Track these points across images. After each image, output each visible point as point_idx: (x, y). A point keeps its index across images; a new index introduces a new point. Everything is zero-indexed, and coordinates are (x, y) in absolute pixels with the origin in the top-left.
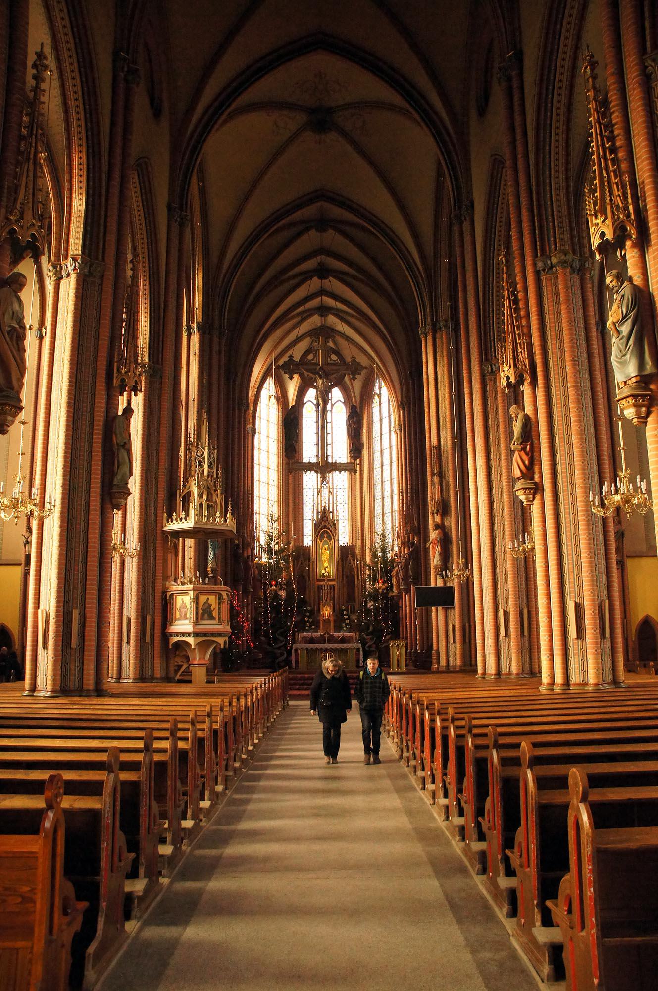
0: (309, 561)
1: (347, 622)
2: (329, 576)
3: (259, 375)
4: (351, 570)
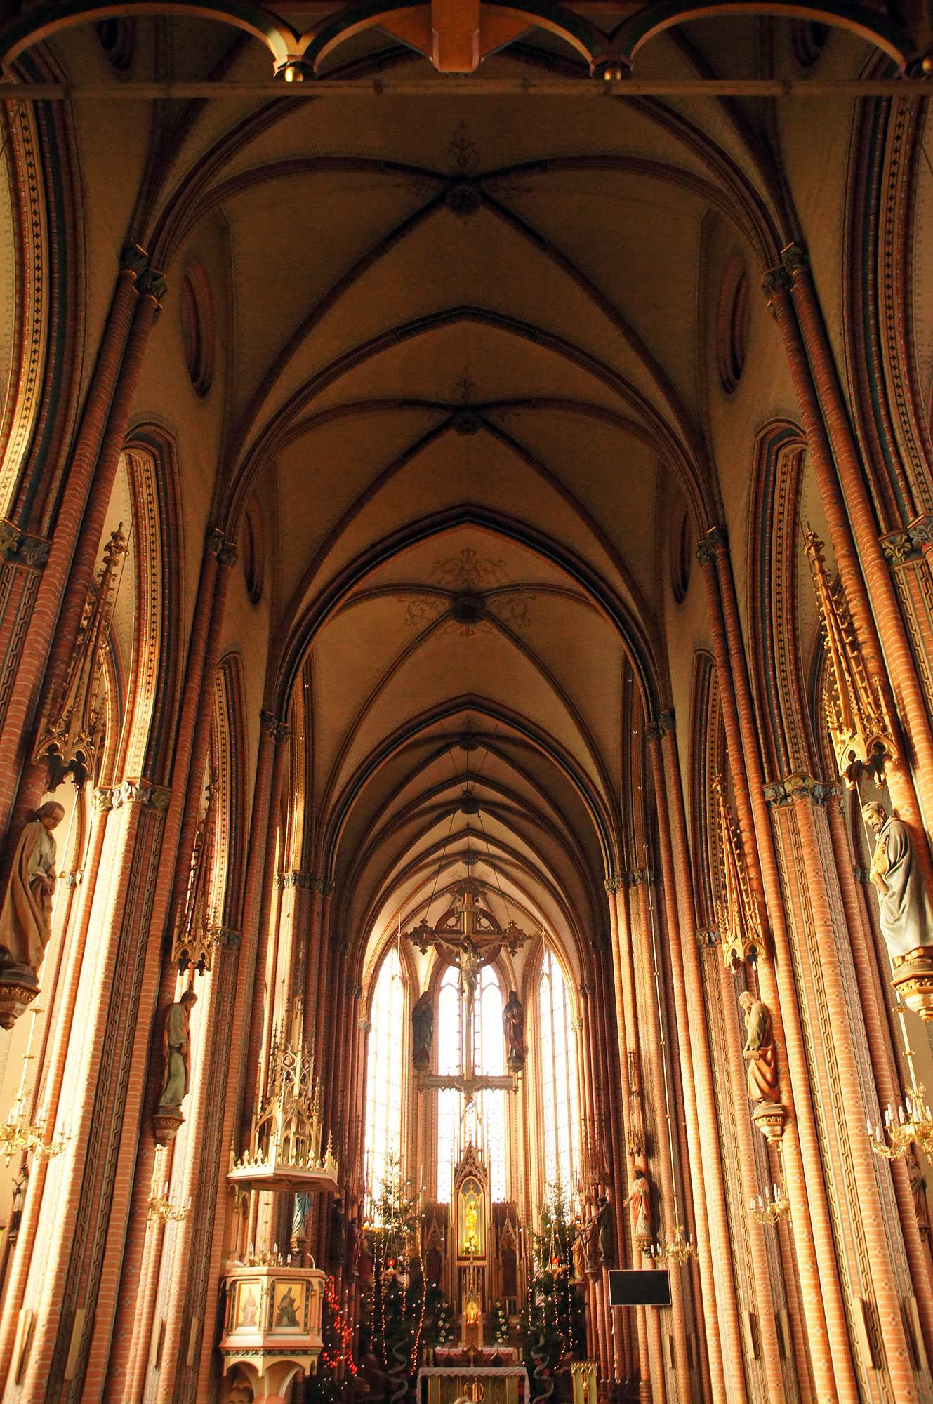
0: (446, 1228)
1: (504, 1328)
4: (510, 1242)
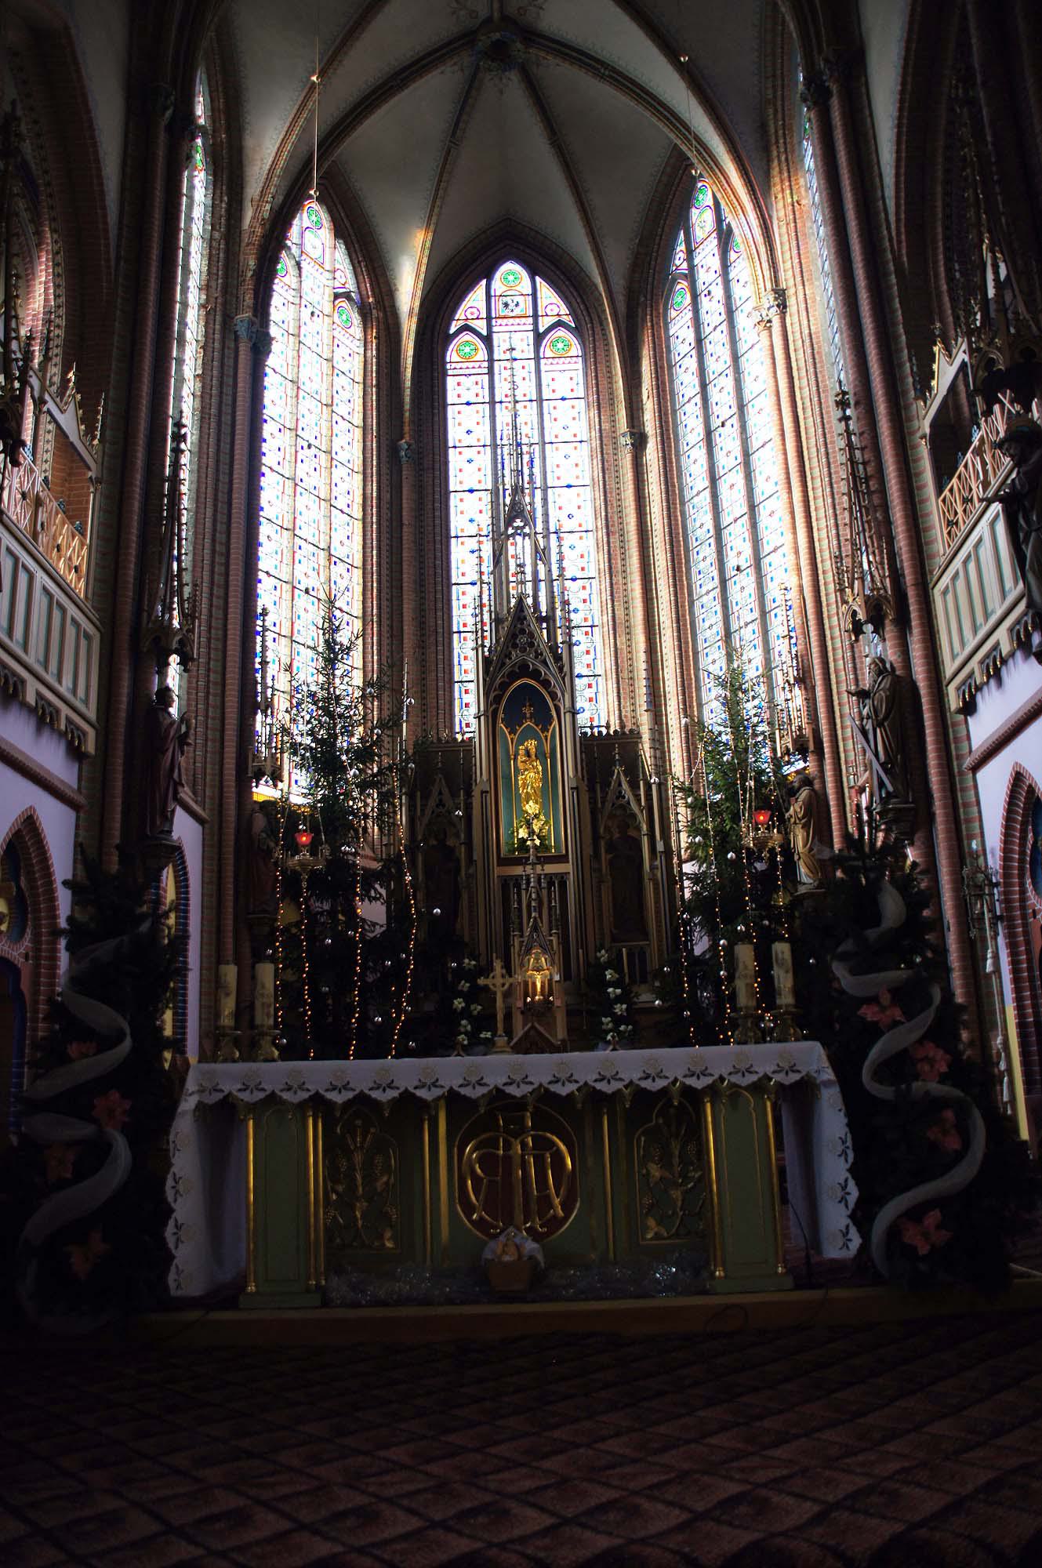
0: (469, 794)
1: (620, 1009)
2: (544, 846)
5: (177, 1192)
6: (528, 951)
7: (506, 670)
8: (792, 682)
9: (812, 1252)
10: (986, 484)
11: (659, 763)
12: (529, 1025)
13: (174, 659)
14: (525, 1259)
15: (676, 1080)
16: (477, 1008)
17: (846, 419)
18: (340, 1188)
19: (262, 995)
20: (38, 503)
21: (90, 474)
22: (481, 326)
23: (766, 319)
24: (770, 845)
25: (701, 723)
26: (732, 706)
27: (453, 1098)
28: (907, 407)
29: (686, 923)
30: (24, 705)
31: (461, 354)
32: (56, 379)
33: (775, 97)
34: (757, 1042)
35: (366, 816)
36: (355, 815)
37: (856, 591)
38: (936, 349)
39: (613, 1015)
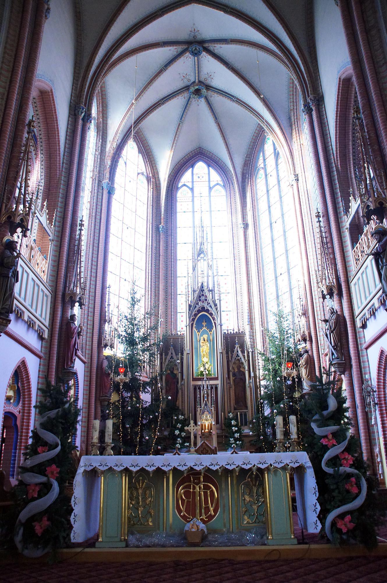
0: (182, 354)
1: (237, 435)
2: (209, 374)
3: (120, 125)
4: (240, 364)
5: (75, 503)
6: (203, 413)
7: (197, 309)
8: (301, 315)
9: (304, 531)
10: (369, 247)
11: (252, 344)
12: (203, 442)
13: (77, 304)
14: (200, 530)
15: (255, 465)
16: (183, 434)
17: (319, 222)
18: (133, 502)
19: (108, 431)
20: (32, 249)
21: (50, 238)
22: (190, 185)
23: (291, 184)
24: (292, 375)
25: (267, 330)
26: (279, 323)
27: (175, 470)
28: (341, 218)
29: (262, 404)
30: (23, 320)
31: (183, 195)
32: (40, 205)
33: (294, 109)
34: (284, 452)
35: (144, 362)
36: (140, 361)
37: (323, 284)
38: (350, 198)
39: (234, 438)
